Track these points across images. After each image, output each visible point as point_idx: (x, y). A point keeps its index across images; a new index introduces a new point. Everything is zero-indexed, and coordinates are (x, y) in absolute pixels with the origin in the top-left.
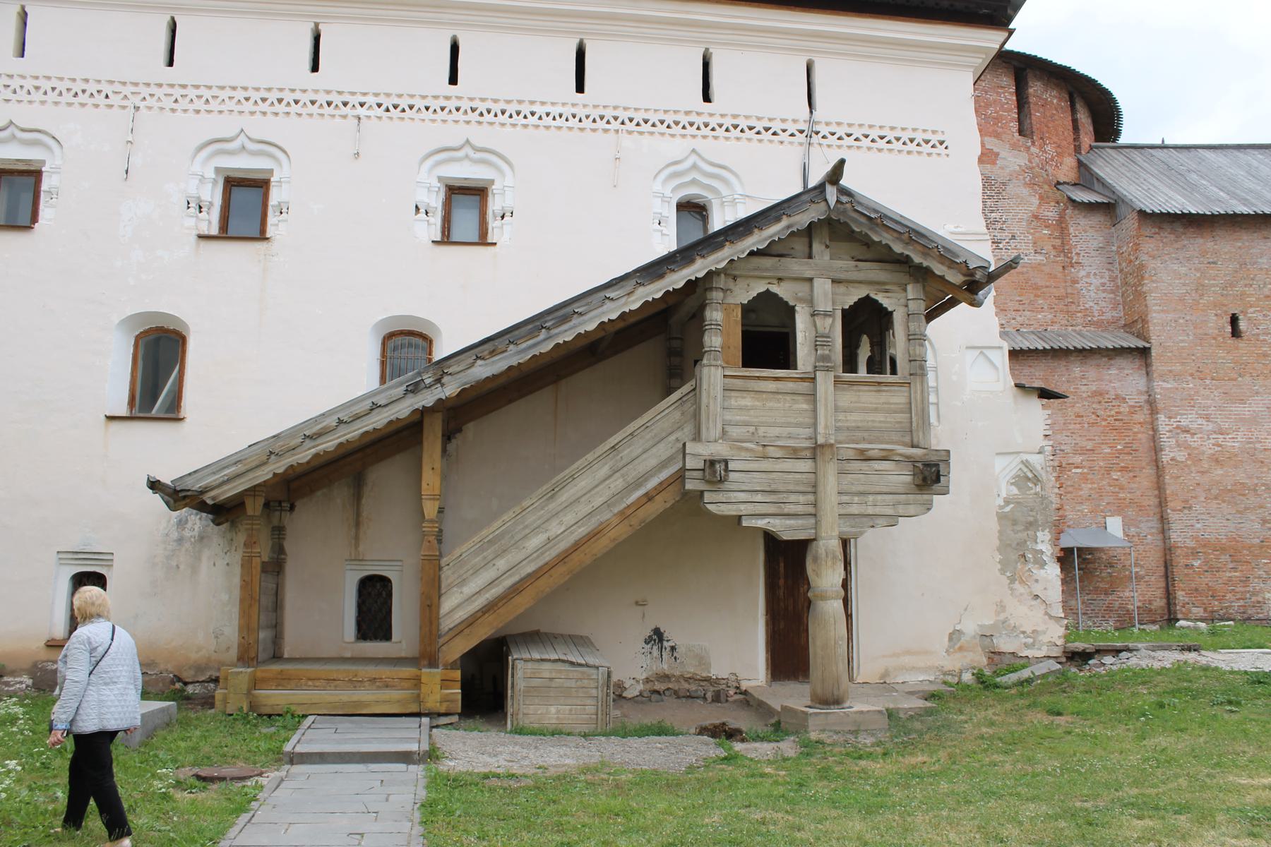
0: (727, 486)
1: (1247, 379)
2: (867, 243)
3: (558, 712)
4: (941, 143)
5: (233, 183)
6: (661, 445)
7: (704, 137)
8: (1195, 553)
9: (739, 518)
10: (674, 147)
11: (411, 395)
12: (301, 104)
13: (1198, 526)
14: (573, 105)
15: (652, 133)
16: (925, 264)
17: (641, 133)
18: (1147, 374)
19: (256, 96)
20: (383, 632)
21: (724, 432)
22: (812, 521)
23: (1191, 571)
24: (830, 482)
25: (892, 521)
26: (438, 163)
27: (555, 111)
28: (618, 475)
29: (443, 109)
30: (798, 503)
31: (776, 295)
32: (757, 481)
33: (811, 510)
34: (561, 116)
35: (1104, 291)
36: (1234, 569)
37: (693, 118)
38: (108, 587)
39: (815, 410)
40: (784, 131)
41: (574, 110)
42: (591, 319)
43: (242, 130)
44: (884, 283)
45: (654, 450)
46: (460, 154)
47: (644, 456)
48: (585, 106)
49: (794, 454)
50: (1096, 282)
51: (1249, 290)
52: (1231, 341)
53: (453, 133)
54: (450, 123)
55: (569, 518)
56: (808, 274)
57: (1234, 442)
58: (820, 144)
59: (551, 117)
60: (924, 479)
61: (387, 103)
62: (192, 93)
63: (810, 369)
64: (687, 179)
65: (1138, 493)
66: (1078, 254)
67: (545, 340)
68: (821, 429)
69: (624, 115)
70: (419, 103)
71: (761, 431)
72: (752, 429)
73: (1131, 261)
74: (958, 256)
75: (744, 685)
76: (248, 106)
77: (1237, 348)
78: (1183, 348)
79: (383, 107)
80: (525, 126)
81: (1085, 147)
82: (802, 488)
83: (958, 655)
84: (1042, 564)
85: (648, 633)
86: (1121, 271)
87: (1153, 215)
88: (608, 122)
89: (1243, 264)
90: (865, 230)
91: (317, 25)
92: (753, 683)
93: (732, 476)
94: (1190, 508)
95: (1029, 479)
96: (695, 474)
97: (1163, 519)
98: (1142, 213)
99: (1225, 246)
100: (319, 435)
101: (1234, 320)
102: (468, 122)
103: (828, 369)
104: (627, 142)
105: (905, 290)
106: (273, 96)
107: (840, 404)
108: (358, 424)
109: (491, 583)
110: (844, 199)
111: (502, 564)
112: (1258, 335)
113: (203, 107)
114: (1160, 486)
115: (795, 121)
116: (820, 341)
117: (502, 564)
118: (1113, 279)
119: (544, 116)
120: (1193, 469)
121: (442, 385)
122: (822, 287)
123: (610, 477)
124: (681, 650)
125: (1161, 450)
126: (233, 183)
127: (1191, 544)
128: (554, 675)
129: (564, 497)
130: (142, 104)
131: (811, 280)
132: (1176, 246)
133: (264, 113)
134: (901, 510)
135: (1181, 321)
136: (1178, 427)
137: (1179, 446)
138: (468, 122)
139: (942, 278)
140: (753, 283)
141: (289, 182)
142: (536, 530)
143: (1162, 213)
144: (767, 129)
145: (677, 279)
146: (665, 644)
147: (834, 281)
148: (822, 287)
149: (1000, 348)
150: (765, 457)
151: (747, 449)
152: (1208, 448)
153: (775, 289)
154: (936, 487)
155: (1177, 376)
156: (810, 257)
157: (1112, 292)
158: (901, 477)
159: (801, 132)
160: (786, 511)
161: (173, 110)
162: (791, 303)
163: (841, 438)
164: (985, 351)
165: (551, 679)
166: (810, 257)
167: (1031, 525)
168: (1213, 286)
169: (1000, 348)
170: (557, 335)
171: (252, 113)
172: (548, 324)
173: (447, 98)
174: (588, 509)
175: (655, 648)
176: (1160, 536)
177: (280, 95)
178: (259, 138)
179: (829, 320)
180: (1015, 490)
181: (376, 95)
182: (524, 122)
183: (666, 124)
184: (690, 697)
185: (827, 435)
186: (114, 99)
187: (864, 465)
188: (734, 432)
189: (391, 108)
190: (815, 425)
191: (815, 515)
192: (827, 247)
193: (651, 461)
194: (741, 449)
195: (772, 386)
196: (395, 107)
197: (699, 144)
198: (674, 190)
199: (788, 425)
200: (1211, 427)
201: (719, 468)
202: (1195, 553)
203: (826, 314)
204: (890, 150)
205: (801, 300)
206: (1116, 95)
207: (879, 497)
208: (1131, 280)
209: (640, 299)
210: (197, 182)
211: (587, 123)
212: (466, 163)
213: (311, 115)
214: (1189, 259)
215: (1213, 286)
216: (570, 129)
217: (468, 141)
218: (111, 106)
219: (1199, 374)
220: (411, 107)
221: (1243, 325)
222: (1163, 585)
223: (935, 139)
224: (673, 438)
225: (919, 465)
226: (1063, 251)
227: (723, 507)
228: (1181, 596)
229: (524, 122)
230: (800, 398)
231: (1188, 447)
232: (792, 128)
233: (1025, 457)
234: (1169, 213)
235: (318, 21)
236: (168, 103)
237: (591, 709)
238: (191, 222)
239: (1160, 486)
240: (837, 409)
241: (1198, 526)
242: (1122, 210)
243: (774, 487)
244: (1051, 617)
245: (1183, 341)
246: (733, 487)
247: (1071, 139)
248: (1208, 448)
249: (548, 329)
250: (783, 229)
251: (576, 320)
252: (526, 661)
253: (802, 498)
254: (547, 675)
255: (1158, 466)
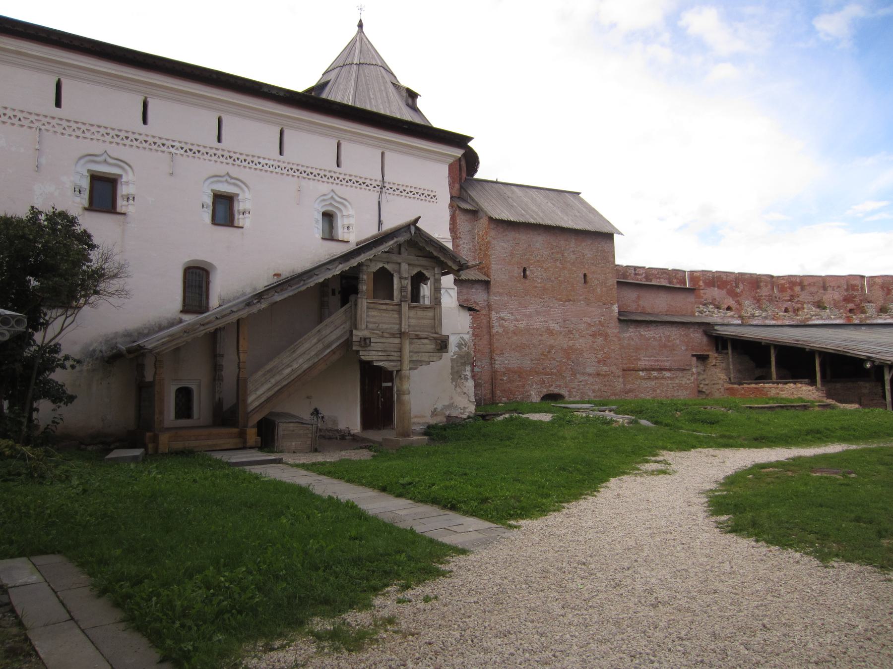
0: (368, 348)
1: (528, 297)
2: (422, 249)
3: (296, 444)
4: (435, 196)
5: (96, 179)
6: (338, 330)
7: (337, 184)
8: (504, 374)
9: (372, 361)
10: (324, 188)
11: (247, 307)
12: (139, 141)
13: (506, 362)
14: (279, 161)
15: (314, 180)
16: (445, 261)
17: (309, 179)
18: (488, 292)
19: (113, 133)
20: (189, 415)
21: (367, 326)
22: (399, 363)
23: (502, 382)
24: (407, 348)
25: (428, 363)
26: (212, 182)
27: (270, 163)
28: (321, 342)
29: (215, 155)
30: (394, 356)
31: (386, 269)
32: (379, 347)
33: (399, 358)
34: (272, 166)
35: (470, 252)
36: (520, 381)
37: (332, 174)
38: (74, 395)
39: (400, 318)
40: (371, 185)
41: (279, 164)
42: (321, 278)
43: (106, 151)
44: (425, 266)
45: (335, 332)
46: (224, 179)
47: (331, 334)
48: (284, 162)
49: (393, 335)
50: (467, 247)
51: (531, 258)
52: (523, 280)
53: (222, 169)
54: (218, 163)
55: (301, 361)
56: (399, 261)
57: (522, 325)
58: (386, 193)
59: (268, 166)
60: (441, 347)
61: (186, 147)
62: (74, 126)
63: (398, 300)
64: (328, 203)
65: (482, 347)
66: (460, 233)
67: (303, 285)
68: (403, 326)
69: (302, 169)
70: (203, 150)
71: (380, 325)
72: (377, 325)
73: (483, 239)
74: (457, 258)
75: (352, 432)
76: (108, 138)
77: (525, 283)
78: (504, 282)
79: (184, 150)
80: (256, 169)
81: (463, 179)
82: (396, 350)
83: (435, 418)
84: (467, 379)
85: (312, 411)
86: (478, 243)
87: (496, 220)
88: (294, 172)
89: (530, 245)
90: (424, 245)
91: (146, 98)
92: (355, 431)
93: (372, 344)
94: (503, 354)
95: (463, 345)
96: (357, 343)
97: (491, 358)
98: (491, 219)
99: (523, 237)
100: (207, 323)
101: (525, 270)
102: (227, 163)
103: (406, 301)
104: (304, 183)
105: (434, 269)
106: (123, 134)
107: (410, 315)
108: (224, 319)
109: (269, 389)
110: (417, 232)
111: (273, 381)
112: (533, 278)
113: (82, 135)
114: (490, 344)
115: (376, 180)
116: (402, 289)
117: (273, 381)
118: (474, 246)
119: (265, 165)
120: (505, 337)
121: (261, 303)
122: (405, 266)
123: (317, 343)
124: (326, 418)
125: (493, 327)
126: (96, 179)
127: (504, 370)
128: (295, 429)
129: (299, 352)
130: (43, 128)
131: (400, 264)
132: (504, 234)
133: (118, 144)
134: (431, 359)
135: (503, 269)
136: (500, 317)
137: (500, 326)
138: (227, 163)
139: (451, 267)
140: (378, 263)
141: (134, 184)
142: (288, 366)
143: (499, 219)
144: (364, 183)
145: (354, 262)
146: (320, 415)
147: (409, 265)
148: (405, 266)
149: (454, 289)
150: (383, 337)
151: (376, 334)
152: (512, 327)
153: (386, 266)
154: (445, 350)
155: (501, 294)
156: (400, 253)
157: (474, 252)
158: (430, 346)
159: (378, 186)
160: (390, 359)
161: (62, 134)
162: (392, 273)
163: (410, 330)
164: (449, 291)
165: (293, 430)
166: (400, 253)
167: (464, 364)
168: (518, 254)
169: (454, 289)
170: (307, 283)
171: (111, 143)
172: (304, 279)
173: (217, 149)
174: (308, 357)
175: (315, 417)
176: (490, 366)
177: (127, 135)
178: (116, 157)
179: (407, 281)
180: (457, 349)
181: (180, 142)
182: (255, 167)
183: (320, 176)
184: (330, 438)
185: (405, 328)
186: (23, 122)
187: (418, 341)
188: (370, 326)
189: (188, 151)
190: (400, 324)
191: (400, 361)
192: (407, 250)
193: (333, 337)
194: (374, 333)
195: (384, 307)
196: (191, 150)
197: (334, 187)
198: (323, 207)
199: (391, 323)
200: (513, 318)
201: (368, 341)
202: (504, 374)
203: (406, 278)
204: (414, 198)
205: (395, 271)
206: (479, 155)
207: (423, 354)
208: (483, 248)
209: (340, 270)
210: (79, 177)
211: (285, 171)
212: (226, 185)
213: (145, 148)
214: (508, 241)
215: (518, 254)
216: (277, 173)
217: (228, 174)
218: (22, 126)
219: (509, 294)
220: (199, 152)
221: (528, 273)
222: (490, 388)
223: (432, 194)
224: (342, 327)
225: (439, 341)
226: (453, 231)
227: (367, 357)
228: (498, 393)
229: (255, 167)
230: (395, 312)
231: (503, 326)
232: (375, 184)
233: (462, 335)
234: (502, 220)
235: (146, 96)
236: (59, 129)
237: (309, 442)
238: (78, 200)
239: (490, 344)
240: (409, 318)
241: (506, 362)
242: (481, 214)
243: (386, 349)
244: (470, 401)
245: (504, 278)
246: (372, 349)
247: (458, 175)
248: (512, 327)
249: (304, 281)
250: (394, 243)
251: (315, 277)
252: (283, 423)
253: (396, 354)
254: (291, 428)
255: (490, 335)
